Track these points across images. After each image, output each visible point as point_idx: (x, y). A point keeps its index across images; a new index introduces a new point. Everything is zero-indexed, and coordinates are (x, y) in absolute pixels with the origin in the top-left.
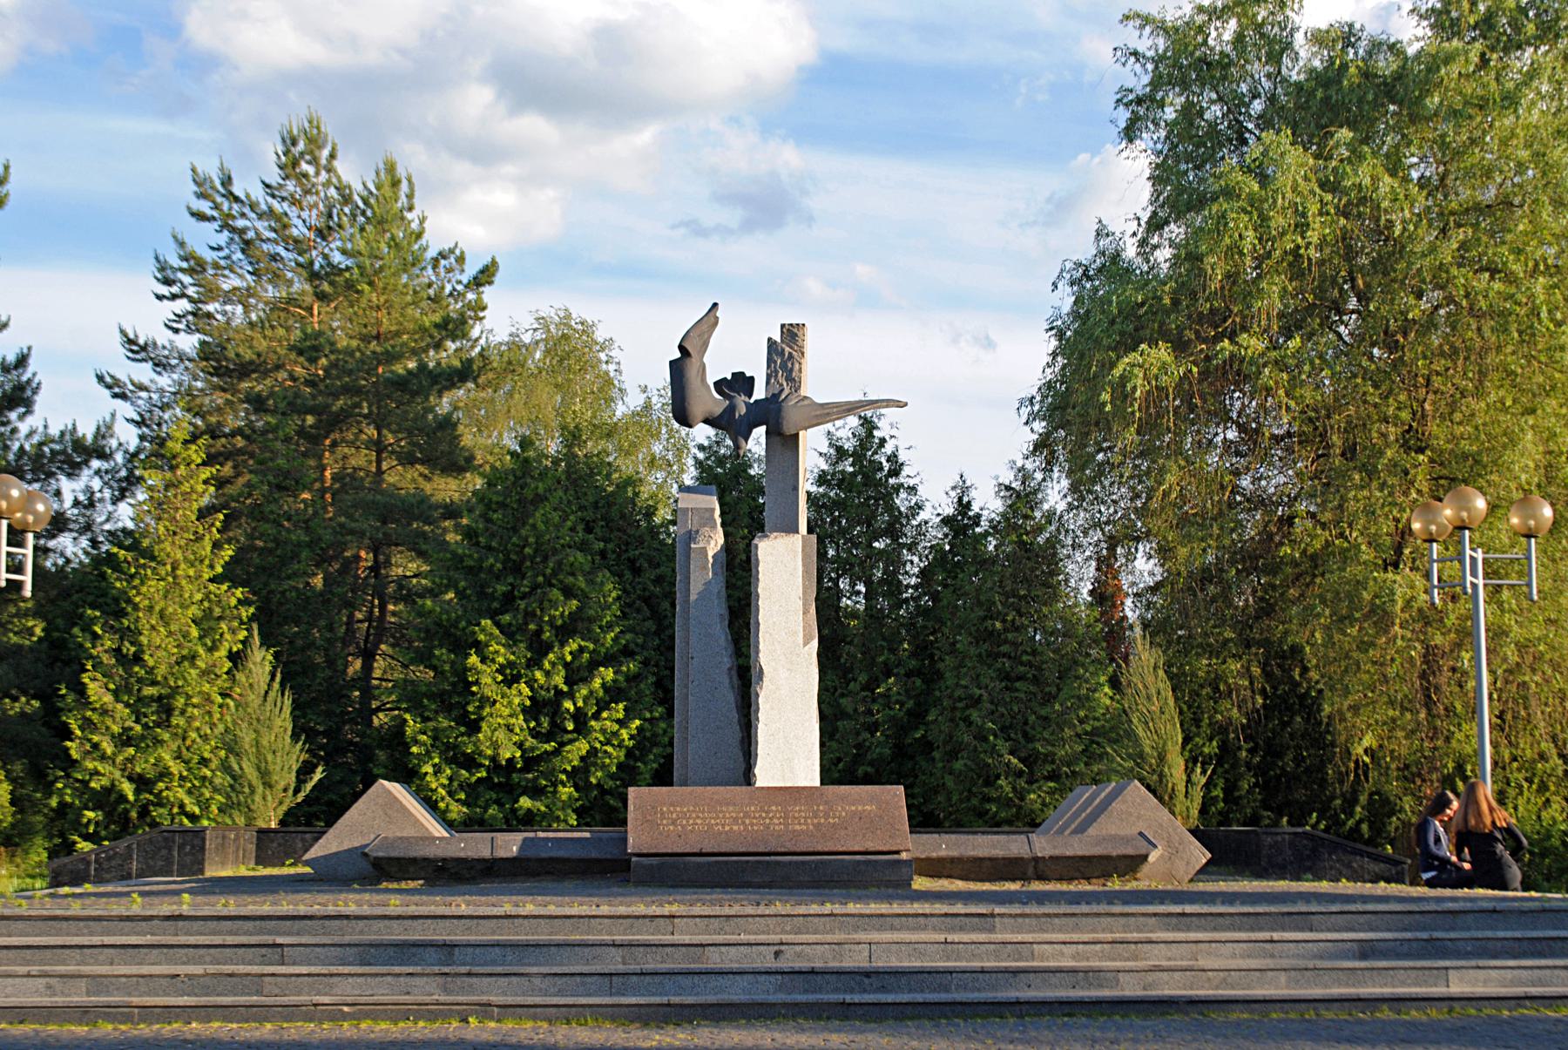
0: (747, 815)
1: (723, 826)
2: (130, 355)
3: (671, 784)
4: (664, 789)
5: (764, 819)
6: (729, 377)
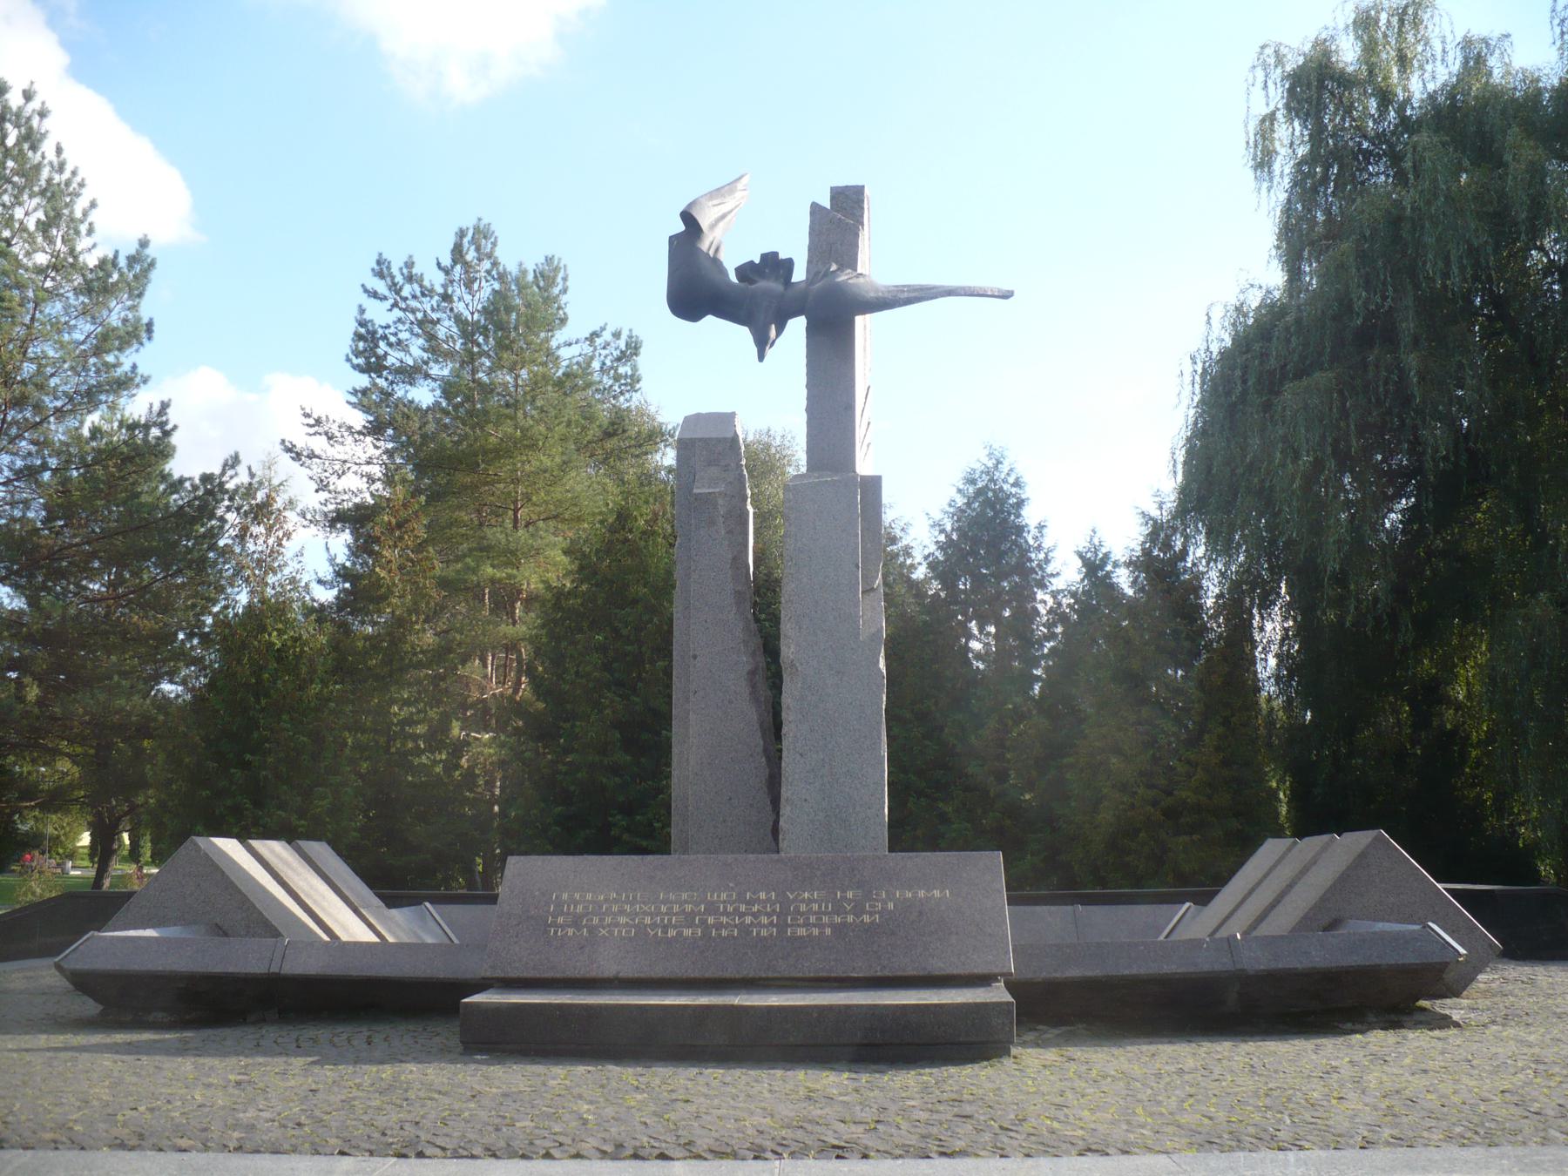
0: (712, 909)
1: (665, 928)
2: (312, 430)
3: (670, 854)
4: (665, 857)
5: (742, 915)
6: (757, 261)
